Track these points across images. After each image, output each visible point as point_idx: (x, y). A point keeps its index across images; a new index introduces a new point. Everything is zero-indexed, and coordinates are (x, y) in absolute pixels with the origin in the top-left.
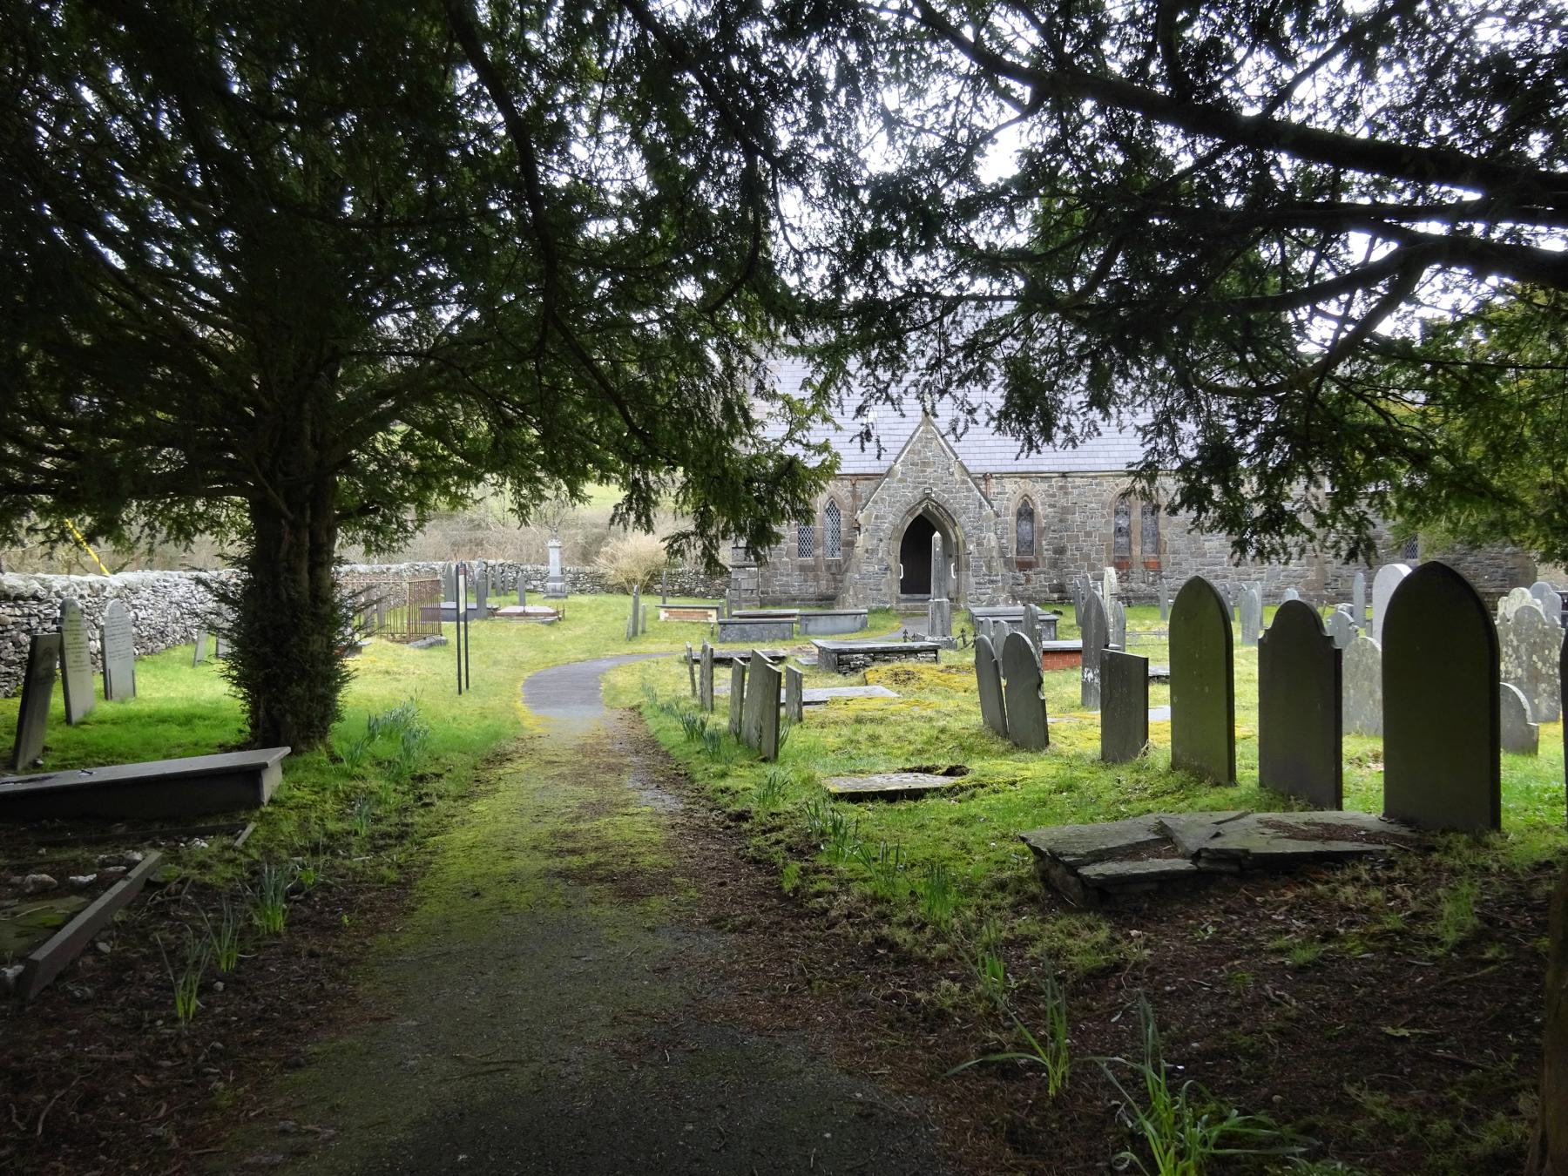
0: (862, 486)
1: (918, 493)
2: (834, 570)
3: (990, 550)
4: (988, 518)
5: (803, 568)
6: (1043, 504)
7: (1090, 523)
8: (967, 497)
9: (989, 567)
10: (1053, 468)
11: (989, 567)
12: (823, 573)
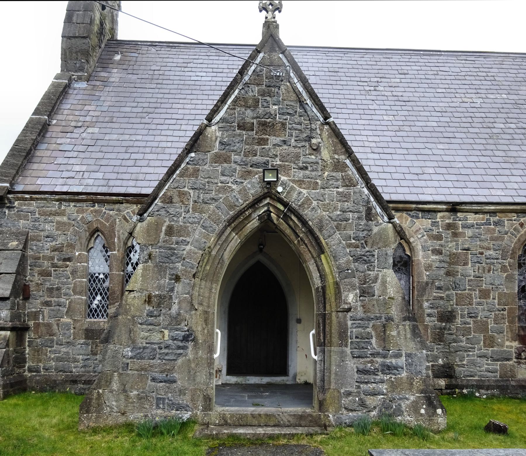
1: (253, 187)
3: (386, 304)
5: (91, 334)
6: (425, 249)
7: (488, 278)
8: (345, 197)
9: (384, 338)
11: (384, 338)
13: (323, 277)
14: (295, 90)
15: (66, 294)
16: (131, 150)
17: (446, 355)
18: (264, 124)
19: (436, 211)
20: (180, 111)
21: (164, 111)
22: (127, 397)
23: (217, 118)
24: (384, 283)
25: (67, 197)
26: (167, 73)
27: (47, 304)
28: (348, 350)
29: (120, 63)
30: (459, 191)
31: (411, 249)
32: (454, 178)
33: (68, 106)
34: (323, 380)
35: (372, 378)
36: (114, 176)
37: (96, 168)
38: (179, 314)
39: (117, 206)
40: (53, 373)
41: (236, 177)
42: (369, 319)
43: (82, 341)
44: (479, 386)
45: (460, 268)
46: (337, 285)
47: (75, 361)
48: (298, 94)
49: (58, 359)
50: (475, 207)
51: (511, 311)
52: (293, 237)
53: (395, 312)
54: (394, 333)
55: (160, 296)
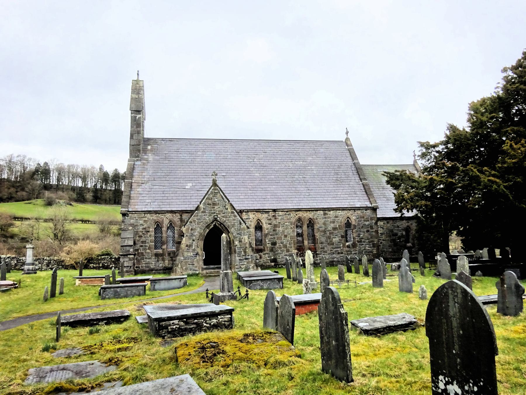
0: (185, 216)
1: (211, 218)
2: (172, 255)
3: (245, 244)
4: (244, 229)
5: (157, 255)
6: (266, 223)
8: (234, 220)
9: (245, 252)
10: (270, 208)
11: (245, 252)
16: (165, 192)
17: (274, 255)
19: (269, 212)
20: (180, 174)
21: (173, 174)
23: (202, 203)
26: (171, 155)
27: (141, 246)
29: (151, 150)
30: (277, 205)
31: (262, 223)
33: (137, 174)
36: (161, 204)
37: (154, 201)
40: (144, 268)
45: (277, 229)
48: (222, 196)
49: (146, 264)
53: (247, 246)
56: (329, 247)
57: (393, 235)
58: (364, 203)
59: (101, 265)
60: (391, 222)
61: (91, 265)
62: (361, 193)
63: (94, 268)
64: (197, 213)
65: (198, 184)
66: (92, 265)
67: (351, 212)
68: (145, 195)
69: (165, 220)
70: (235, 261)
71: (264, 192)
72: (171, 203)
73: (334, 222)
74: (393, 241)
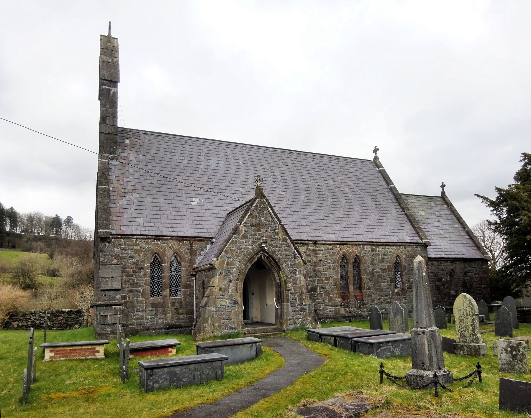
0: (196, 245)
1: (256, 247)
2: (177, 305)
3: (301, 288)
4: (299, 265)
5: (154, 305)
7: (329, 272)
8: (287, 251)
9: (301, 300)
10: (310, 238)
12: (169, 308)
13: (280, 279)
14: (269, 212)
15: (141, 286)
16: (162, 209)
18: (259, 224)
19: (308, 244)
22: (214, 326)
24: (300, 280)
25: (141, 237)
27: (131, 291)
28: (290, 304)
32: (314, 228)
34: (281, 315)
35: (297, 313)
37: (148, 220)
38: (232, 294)
39: (166, 241)
40: (135, 326)
41: (250, 244)
42: (296, 293)
43: (150, 309)
44: (327, 318)
46: (285, 281)
47: (147, 319)
48: (270, 214)
49: (137, 319)
50: (324, 242)
51: (338, 286)
52: (269, 264)
54: (304, 297)
55: (225, 288)
56: (377, 294)
57: (438, 281)
58: (413, 238)
59: (30, 323)
60: (436, 263)
61: (15, 324)
62: (406, 225)
63: (19, 328)
64: (235, 238)
65: (208, 200)
66: (17, 322)
67: (401, 249)
68: (133, 211)
69: (168, 250)
70: (288, 313)
71: (296, 216)
72: (174, 226)
73: (382, 262)
74: (438, 287)
